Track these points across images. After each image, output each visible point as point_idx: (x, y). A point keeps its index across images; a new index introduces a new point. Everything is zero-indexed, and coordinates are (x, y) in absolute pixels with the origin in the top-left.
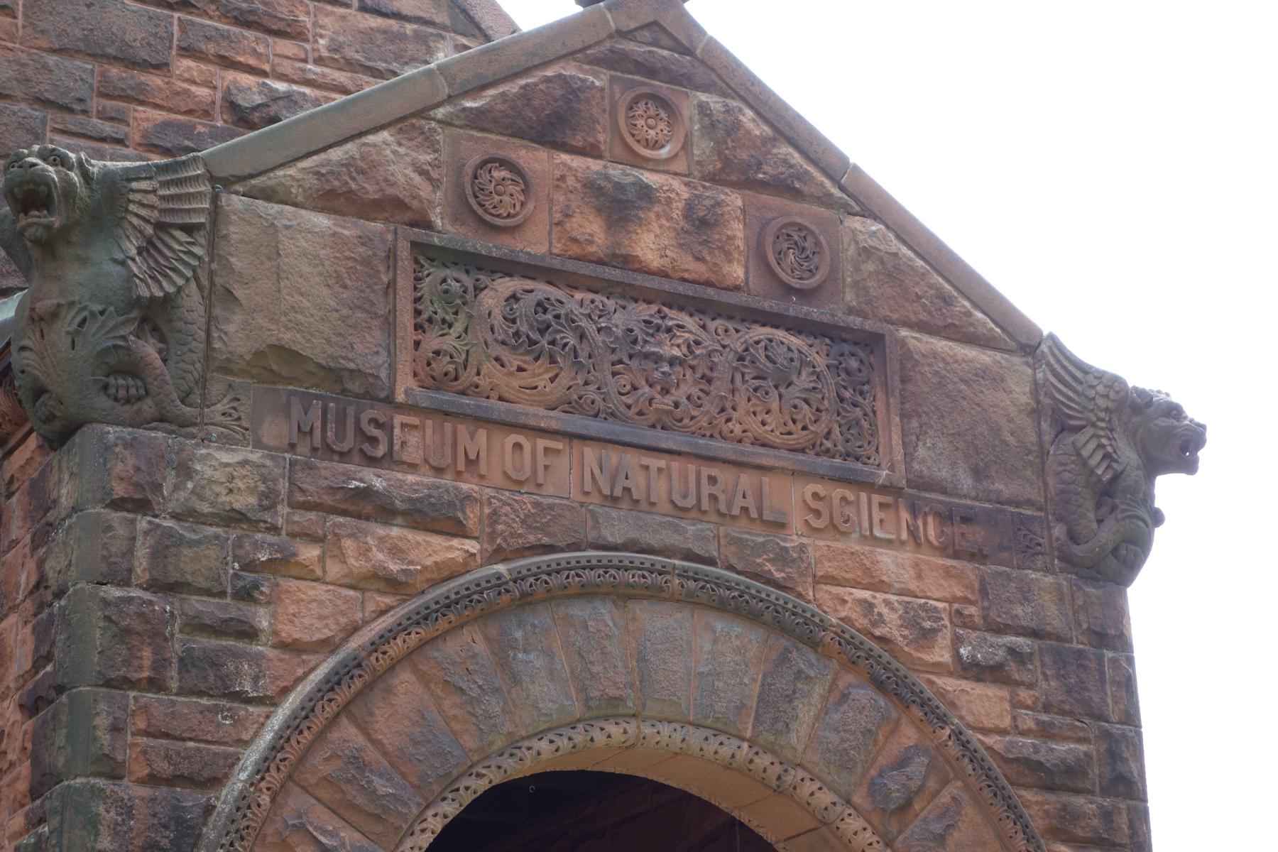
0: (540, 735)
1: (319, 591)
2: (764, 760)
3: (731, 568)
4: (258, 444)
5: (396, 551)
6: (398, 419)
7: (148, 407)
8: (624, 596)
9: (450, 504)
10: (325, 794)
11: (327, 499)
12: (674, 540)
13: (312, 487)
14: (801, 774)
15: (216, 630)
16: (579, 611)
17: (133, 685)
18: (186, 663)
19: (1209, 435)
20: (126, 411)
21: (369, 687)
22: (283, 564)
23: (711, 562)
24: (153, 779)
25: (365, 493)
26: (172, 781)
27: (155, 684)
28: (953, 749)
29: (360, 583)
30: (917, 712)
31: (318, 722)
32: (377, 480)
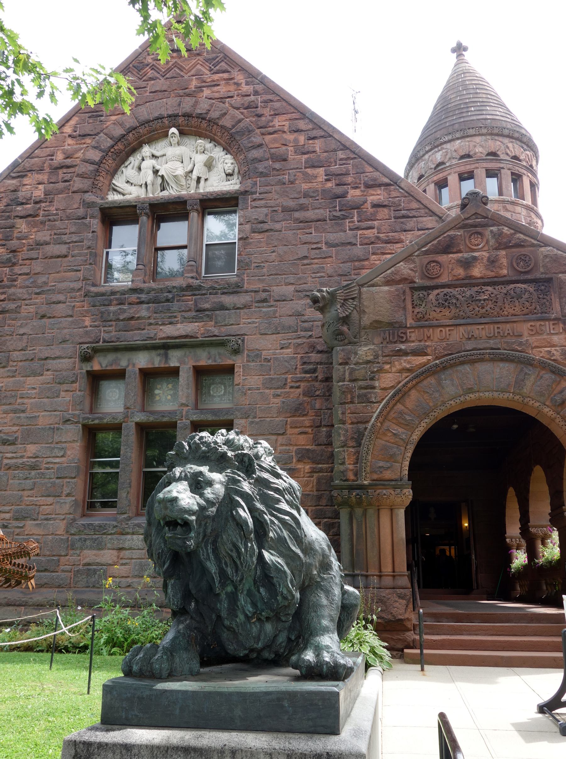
0: (451, 400)
1: (390, 375)
2: (518, 397)
3: (505, 350)
4: (374, 344)
5: (409, 362)
6: (408, 331)
7: (346, 341)
8: (472, 362)
9: (423, 349)
10: (394, 421)
11: (391, 353)
12: (488, 345)
13: (387, 351)
14: (529, 399)
15: (366, 388)
16: (460, 368)
17: (347, 403)
18: (359, 396)
20: (341, 343)
22: (381, 370)
23: (499, 349)
24: (352, 423)
25: (400, 350)
26: (358, 423)
27: (352, 402)
29: (401, 371)
31: (391, 405)
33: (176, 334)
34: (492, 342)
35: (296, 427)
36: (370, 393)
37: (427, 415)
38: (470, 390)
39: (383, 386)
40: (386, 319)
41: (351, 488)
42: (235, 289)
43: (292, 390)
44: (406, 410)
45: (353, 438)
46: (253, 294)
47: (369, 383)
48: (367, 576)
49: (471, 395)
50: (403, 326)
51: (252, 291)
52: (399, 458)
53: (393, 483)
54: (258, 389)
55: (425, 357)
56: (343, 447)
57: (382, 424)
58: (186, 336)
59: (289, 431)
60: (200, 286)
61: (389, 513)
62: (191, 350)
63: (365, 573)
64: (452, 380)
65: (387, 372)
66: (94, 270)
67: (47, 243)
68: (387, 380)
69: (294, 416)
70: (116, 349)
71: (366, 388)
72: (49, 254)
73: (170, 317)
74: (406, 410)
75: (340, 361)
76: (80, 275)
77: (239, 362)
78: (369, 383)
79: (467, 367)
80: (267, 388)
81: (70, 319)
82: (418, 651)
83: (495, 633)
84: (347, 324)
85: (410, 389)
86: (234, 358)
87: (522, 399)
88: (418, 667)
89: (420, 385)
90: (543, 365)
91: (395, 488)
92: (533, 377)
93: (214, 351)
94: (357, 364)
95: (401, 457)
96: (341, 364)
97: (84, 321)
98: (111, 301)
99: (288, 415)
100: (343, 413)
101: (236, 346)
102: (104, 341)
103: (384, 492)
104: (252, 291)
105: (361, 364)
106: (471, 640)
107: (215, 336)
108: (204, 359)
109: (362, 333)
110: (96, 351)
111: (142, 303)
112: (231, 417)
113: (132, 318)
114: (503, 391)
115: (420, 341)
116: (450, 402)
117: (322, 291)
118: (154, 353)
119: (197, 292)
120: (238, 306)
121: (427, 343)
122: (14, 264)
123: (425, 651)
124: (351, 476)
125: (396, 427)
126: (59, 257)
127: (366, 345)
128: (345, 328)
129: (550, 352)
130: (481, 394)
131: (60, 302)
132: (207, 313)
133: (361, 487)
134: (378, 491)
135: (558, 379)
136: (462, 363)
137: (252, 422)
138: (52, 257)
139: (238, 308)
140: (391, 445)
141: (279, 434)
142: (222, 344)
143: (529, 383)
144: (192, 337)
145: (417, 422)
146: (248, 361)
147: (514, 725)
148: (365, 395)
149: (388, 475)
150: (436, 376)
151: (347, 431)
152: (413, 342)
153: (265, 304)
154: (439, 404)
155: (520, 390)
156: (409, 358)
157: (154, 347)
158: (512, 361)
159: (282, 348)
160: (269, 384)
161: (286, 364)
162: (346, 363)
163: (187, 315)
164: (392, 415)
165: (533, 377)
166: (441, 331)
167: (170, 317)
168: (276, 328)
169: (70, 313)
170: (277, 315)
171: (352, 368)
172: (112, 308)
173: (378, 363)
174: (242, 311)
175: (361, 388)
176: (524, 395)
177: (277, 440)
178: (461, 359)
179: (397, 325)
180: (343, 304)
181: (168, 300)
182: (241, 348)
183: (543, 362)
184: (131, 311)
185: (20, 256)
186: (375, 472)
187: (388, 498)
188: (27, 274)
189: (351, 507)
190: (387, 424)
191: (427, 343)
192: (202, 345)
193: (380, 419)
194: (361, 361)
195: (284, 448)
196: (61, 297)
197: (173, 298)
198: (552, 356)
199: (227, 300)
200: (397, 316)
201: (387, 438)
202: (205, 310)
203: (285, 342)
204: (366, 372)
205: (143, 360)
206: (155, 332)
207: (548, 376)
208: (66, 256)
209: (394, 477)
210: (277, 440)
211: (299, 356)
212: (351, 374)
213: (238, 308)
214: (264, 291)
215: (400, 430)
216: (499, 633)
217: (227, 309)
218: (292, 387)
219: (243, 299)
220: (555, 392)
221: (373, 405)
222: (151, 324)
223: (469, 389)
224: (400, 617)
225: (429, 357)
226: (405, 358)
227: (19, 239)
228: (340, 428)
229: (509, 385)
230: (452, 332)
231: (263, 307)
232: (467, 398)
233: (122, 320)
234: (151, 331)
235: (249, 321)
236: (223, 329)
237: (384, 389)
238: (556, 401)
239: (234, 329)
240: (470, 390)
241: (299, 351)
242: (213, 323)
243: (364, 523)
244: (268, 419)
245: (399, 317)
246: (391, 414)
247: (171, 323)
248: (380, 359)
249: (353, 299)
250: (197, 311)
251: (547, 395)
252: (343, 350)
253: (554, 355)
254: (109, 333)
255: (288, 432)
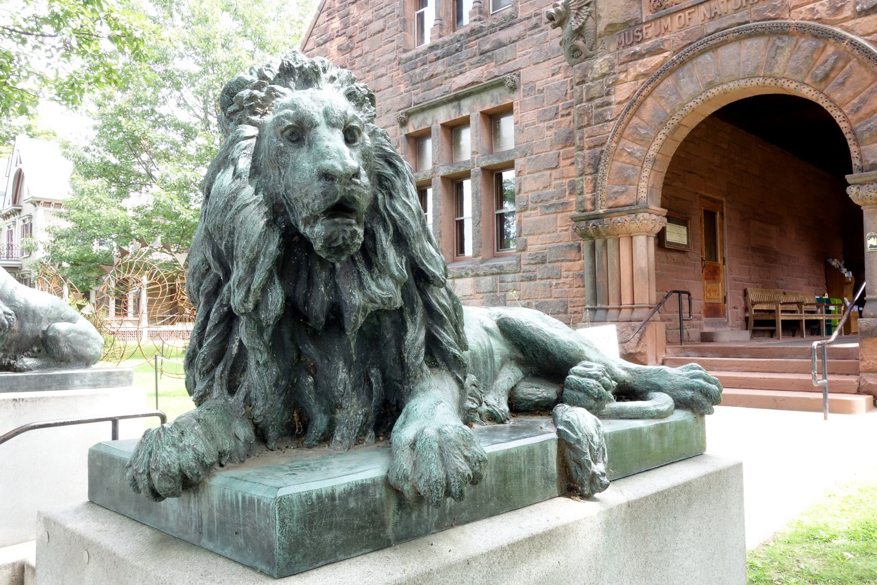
0: (690, 101)
1: (626, 85)
2: (769, 81)
3: (755, 21)
4: (610, 52)
5: (645, 65)
6: (644, 27)
7: (583, 56)
8: (714, 48)
9: (659, 45)
10: (630, 138)
11: (626, 59)
12: (733, 21)
13: (622, 58)
14: (783, 80)
15: (602, 105)
16: (701, 59)
17: (585, 126)
18: (596, 116)
19: (744, 465)
20: (579, 60)
21: (639, 107)
22: (616, 82)
23: (747, 22)
24: (589, 148)
25: (635, 53)
26: (595, 146)
27: (589, 125)
28: (849, 48)
29: (636, 78)
30: (832, 40)
31: (625, 120)
32: (637, 48)
33: (464, 83)
34: (738, 15)
35: (568, 158)
36: (605, 111)
37: (663, 124)
38: (711, 85)
39: (619, 99)
40: (619, 20)
41: (588, 219)
42: (510, 22)
43: (563, 119)
44: (642, 123)
45: (590, 164)
46: (526, 22)
47: (605, 99)
48: (607, 310)
49: (713, 90)
50: (638, 23)
51: (525, 19)
52: (634, 180)
53: (627, 208)
54: (534, 124)
55: (662, 55)
56: (581, 175)
57: (617, 143)
58: (473, 83)
59: (563, 163)
60: (482, 27)
61: (628, 241)
62: (478, 96)
63: (604, 306)
64: (691, 76)
65: (624, 82)
66: (405, 35)
67: (371, 22)
68: (623, 92)
69: (565, 147)
70: (422, 110)
71: (602, 105)
72: (373, 32)
73: (460, 67)
74: (642, 123)
75: (577, 81)
76: (394, 44)
77: (516, 99)
78: (605, 99)
79: (708, 57)
80: (541, 121)
81: (391, 89)
82: (820, 396)
83: (749, 369)
84: (582, 36)
85: (646, 97)
86: (512, 95)
87: (774, 82)
88: (821, 415)
89: (657, 90)
90: (802, 30)
91: (630, 213)
92: (788, 49)
93: (496, 92)
94: (593, 80)
95: (637, 178)
96: (578, 84)
97: (399, 88)
98: (416, 63)
99: (560, 146)
100: (581, 139)
101: (511, 84)
102: (415, 104)
103: (619, 219)
104: (525, 19)
105: (597, 79)
106: (781, 379)
107: (496, 76)
108: (489, 102)
109: (599, 43)
110: (409, 115)
111: (438, 59)
112: (511, 158)
113: (432, 76)
114: (751, 78)
115: (657, 36)
116: (690, 104)
117: (557, 5)
118: (450, 106)
119: (479, 35)
120: (513, 39)
121: (664, 37)
122: (352, 49)
123: (831, 396)
124: (589, 206)
125: (631, 145)
126: (379, 32)
127: (602, 56)
128: (580, 43)
129: (813, 9)
130: (725, 87)
131: (383, 75)
132: (488, 54)
133: (598, 217)
134: (614, 219)
135: (822, 45)
136: (703, 52)
137: (529, 160)
138: (375, 34)
139: (514, 41)
140: (627, 166)
141: (553, 168)
142: (501, 84)
143: (782, 60)
144: (477, 83)
145: (653, 135)
146: (524, 96)
147: (739, 466)
148: (601, 114)
149: (623, 200)
150: (674, 75)
151: (584, 157)
152: (650, 39)
153: (536, 30)
154: (677, 108)
155: (771, 70)
156: (645, 60)
157: (450, 101)
158: (762, 34)
159: (553, 75)
160: (542, 117)
161: (557, 91)
162: (583, 82)
163: (472, 61)
164: (627, 131)
165: (788, 49)
166: (680, 17)
167: (460, 67)
168: (547, 53)
169: (390, 84)
170: (548, 39)
171: (588, 86)
172: (417, 71)
173: (614, 73)
174: (517, 43)
175: (598, 107)
176: (778, 76)
177: (551, 175)
178: (701, 47)
179: (633, 24)
180: (577, 14)
181: (457, 50)
182: (517, 84)
183: (802, 27)
184: (431, 69)
185: (356, 39)
186: (610, 198)
187: (623, 225)
188: (361, 55)
189: (592, 238)
190: (623, 142)
191: (664, 37)
192: (485, 89)
193: (615, 139)
194: (597, 76)
195: (558, 181)
196: (382, 71)
197: (461, 46)
198: (814, 15)
199: (503, 35)
200: (632, 12)
201: (623, 159)
202: (486, 52)
203: (556, 67)
204: (602, 87)
205: (444, 115)
206: (449, 85)
207: (806, 44)
208: (383, 30)
209: (630, 201)
210: (551, 175)
211: (569, 79)
212: (587, 93)
213: (514, 41)
214: (536, 15)
215: (636, 147)
216: (754, 369)
217: (505, 45)
218: (563, 116)
219: (518, 29)
220: (818, 64)
221: (608, 124)
222: (446, 78)
223: (710, 83)
224: (633, 351)
225: (666, 54)
226: (640, 61)
227: (353, 24)
228: (578, 155)
229: (757, 68)
230: (693, 15)
231: (535, 34)
232: (709, 94)
233: (426, 80)
234: (446, 87)
235: (523, 52)
236: (502, 68)
237: (620, 103)
238: (816, 77)
239: (511, 66)
240: (711, 85)
241: (568, 74)
242: (493, 64)
243: (604, 254)
244: (543, 154)
245: (634, 12)
246: (626, 130)
247: (461, 73)
248: (617, 68)
249: (588, 5)
250: (481, 54)
251: (805, 71)
252: (579, 68)
253: (818, 12)
254: (418, 96)
255: (561, 165)
